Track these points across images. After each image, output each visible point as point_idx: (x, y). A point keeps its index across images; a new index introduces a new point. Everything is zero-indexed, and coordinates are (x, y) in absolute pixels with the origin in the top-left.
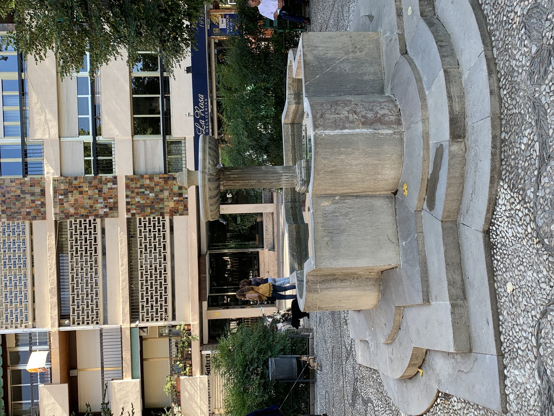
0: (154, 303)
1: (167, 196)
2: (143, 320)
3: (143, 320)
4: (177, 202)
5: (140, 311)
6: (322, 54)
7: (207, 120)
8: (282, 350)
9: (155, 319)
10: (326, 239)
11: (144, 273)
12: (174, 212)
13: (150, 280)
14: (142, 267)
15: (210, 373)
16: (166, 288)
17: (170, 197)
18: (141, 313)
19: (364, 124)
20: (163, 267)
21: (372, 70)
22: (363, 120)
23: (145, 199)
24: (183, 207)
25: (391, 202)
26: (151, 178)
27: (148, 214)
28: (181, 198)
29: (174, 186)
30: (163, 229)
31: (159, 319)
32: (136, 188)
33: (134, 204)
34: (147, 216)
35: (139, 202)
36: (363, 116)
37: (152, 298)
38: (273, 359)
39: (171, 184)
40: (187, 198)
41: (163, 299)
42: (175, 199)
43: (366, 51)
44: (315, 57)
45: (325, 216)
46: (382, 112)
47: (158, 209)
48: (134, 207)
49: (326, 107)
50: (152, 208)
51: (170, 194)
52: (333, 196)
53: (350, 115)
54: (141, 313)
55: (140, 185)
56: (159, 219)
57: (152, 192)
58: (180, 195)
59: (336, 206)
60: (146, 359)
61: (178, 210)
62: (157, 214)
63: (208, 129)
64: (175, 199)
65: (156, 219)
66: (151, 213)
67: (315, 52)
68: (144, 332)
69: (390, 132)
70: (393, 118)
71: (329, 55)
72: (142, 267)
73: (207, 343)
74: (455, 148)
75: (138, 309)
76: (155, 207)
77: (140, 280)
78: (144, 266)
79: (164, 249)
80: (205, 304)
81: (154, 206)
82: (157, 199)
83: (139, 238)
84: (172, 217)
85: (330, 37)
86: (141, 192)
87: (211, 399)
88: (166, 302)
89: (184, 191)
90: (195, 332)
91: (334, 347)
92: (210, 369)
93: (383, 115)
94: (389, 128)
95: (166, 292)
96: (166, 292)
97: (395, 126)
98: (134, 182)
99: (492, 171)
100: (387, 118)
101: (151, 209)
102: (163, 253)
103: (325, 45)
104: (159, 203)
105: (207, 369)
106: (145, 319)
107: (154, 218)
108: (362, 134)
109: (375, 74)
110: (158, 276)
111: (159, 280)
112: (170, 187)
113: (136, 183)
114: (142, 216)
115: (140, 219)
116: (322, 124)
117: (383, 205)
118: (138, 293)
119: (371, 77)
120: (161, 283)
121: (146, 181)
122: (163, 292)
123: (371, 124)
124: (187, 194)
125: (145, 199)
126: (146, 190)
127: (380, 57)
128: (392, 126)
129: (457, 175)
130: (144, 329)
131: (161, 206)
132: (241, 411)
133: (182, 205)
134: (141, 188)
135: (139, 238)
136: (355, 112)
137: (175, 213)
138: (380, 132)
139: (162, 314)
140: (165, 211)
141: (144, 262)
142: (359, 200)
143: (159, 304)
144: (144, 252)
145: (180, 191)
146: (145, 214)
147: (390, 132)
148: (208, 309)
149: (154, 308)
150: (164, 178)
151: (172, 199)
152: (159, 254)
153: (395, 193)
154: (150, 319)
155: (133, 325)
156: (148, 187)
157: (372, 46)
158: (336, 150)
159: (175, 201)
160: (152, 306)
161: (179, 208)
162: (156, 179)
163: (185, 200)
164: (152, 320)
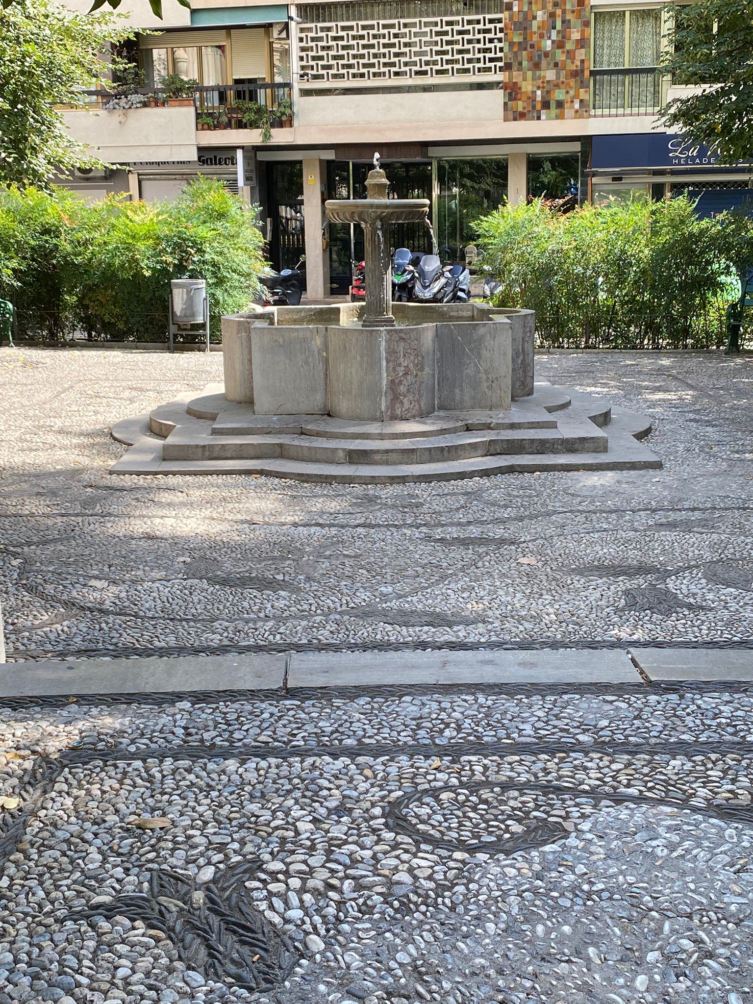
0: (333, 53)
1: (544, 77)
2: (302, 30)
3: (302, 30)
4: (532, 98)
5: (320, 25)
6: (486, 344)
7: (698, 161)
8: (217, 303)
9: (304, 54)
10: (281, 340)
11: (393, 31)
12: (512, 91)
13: (379, 43)
14: (405, 26)
15: (204, 163)
16: (362, 75)
17: (543, 82)
18: (316, 26)
19: (393, 381)
20: (403, 69)
21: (466, 398)
22: (397, 381)
23: (541, 31)
24: (520, 109)
25: (320, 410)
26: (582, 43)
27: (509, 36)
28: (539, 106)
29: (564, 91)
30: (479, 69)
31: (304, 63)
32: (564, 12)
33: (530, 9)
34: (506, 34)
35: (535, 18)
36: (401, 381)
37: (344, 48)
38: (204, 285)
39: (568, 84)
40: (539, 118)
41: (341, 71)
42: (539, 93)
43: (489, 393)
44: (482, 336)
45: (305, 340)
46: (405, 401)
47: (519, 58)
48: (526, 9)
49: (412, 343)
50: (522, 46)
51: (548, 82)
52: (327, 349)
53: (403, 369)
54: (316, 26)
55: (569, 21)
56: (499, 59)
57: (555, 46)
58: (546, 105)
59: (316, 353)
60: (229, 35)
61: (515, 99)
62: (509, 56)
63: (680, 164)
64: (539, 93)
65: (499, 55)
66: (512, 44)
67: (488, 336)
68: (281, 32)
69: (383, 408)
70: (398, 412)
71: (484, 352)
72: (405, 26)
73: (259, 159)
74: (341, 454)
75: (324, 21)
76: (524, 53)
77: (378, 24)
78: (407, 30)
79: (439, 72)
80: (330, 155)
81: (525, 49)
82: (540, 56)
83: (463, 19)
84: (501, 88)
85: (505, 354)
86: (554, 22)
87: (156, 166)
88: (335, 76)
89: (554, 111)
90: (280, 136)
91: (210, 373)
92: (211, 164)
93: (402, 403)
94: (387, 407)
95: (354, 76)
96: (354, 76)
97: (389, 413)
98: (576, 8)
99: (308, 475)
100: (398, 405)
101: (520, 43)
102: (431, 69)
103: (496, 348)
104: (530, 59)
105: (211, 159)
106: (303, 35)
107: (501, 50)
108: (381, 379)
109: (462, 402)
110: (386, 60)
111: (379, 62)
112: (563, 82)
113: (573, 12)
114: (505, 25)
115: (500, 21)
116: (393, 338)
117: (317, 400)
118: (354, 20)
119: (458, 397)
120: (373, 65)
121: (578, 32)
122: (355, 71)
123: (392, 390)
124: (547, 119)
125: (541, 31)
126: (558, 32)
127: (481, 407)
128: (389, 411)
129: (318, 456)
130: (285, 32)
131: (525, 63)
132: (127, 234)
133: (524, 108)
134: (563, 22)
135: (463, 19)
136: (406, 374)
137: (510, 94)
138: (383, 398)
139: (312, 69)
140: (514, 73)
141: (413, 30)
142: (322, 376)
143: (332, 62)
144: (435, 29)
145: (553, 104)
146: (509, 31)
147: (383, 408)
148: (321, 161)
149: (324, 53)
150: (582, 71)
151: (539, 88)
152: (429, 61)
153: (329, 415)
154: (303, 44)
155: (293, 12)
156: (563, 37)
157: (494, 400)
158: (365, 351)
159: (534, 92)
160: (329, 48)
161: (520, 103)
162: (580, 54)
163: (535, 114)
164: (303, 49)
